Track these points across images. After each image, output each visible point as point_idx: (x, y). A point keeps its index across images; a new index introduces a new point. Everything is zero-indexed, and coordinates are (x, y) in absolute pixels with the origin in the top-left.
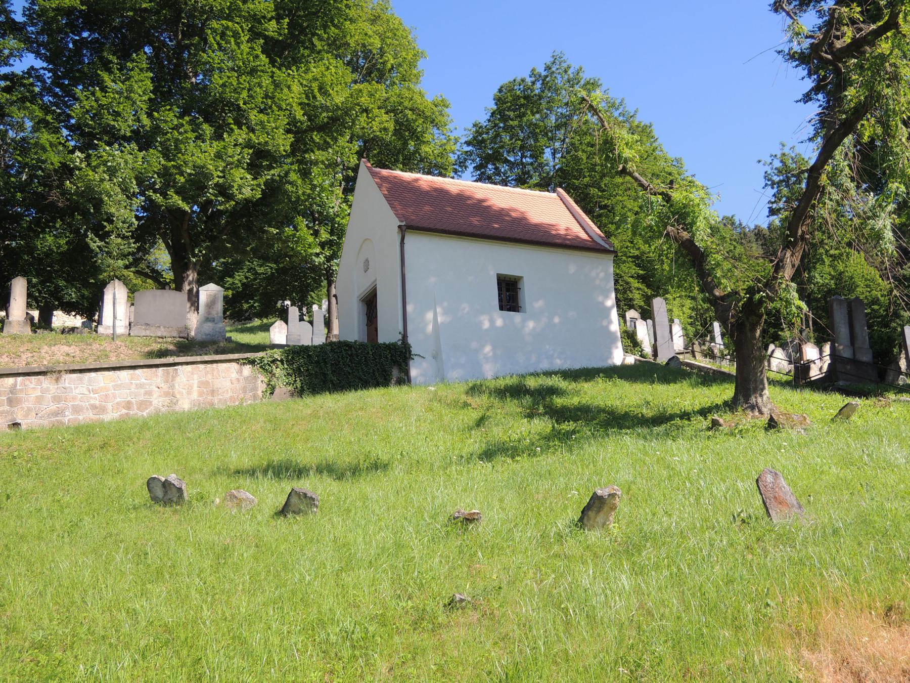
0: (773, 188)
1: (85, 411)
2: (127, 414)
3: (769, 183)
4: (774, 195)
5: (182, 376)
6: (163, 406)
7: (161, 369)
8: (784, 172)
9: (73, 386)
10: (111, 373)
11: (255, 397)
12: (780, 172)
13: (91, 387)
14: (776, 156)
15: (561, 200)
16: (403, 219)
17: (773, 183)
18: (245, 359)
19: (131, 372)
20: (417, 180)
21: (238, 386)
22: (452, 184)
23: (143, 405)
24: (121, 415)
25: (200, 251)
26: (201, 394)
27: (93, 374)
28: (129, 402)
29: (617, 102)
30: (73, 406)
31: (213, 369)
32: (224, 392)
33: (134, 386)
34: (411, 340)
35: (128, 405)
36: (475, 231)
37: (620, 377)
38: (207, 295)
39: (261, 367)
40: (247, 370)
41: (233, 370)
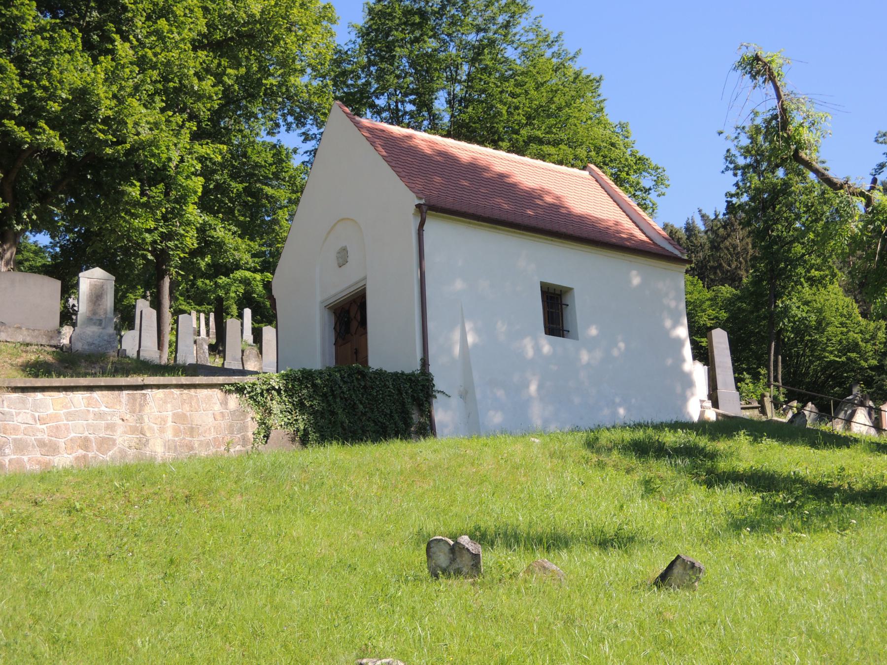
0: (735, 175)
1: (30, 449)
2: (85, 457)
3: (732, 166)
4: (737, 185)
5: (151, 404)
6: (130, 447)
7: (125, 392)
8: (753, 152)
9: (13, 411)
10: (62, 395)
11: (244, 441)
12: (746, 152)
13: (37, 415)
14: (744, 128)
15: (597, 181)
16: (420, 195)
17: (736, 168)
18: (232, 385)
19: (87, 394)
20: (410, 137)
21: (223, 423)
22: (456, 148)
23: (105, 443)
24: (77, 458)
25: (29, 216)
26: (177, 432)
27: (39, 395)
28: (86, 439)
29: (551, 38)
30: (14, 440)
31: (191, 397)
32: (205, 432)
33: (92, 416)
34: (432, 369)
35: (85, 443)
36: (504, 217)
37: (771, 436)
38: (91, 285)
39: (251, 397)
40: (234, 400)
41: (215, 400)
